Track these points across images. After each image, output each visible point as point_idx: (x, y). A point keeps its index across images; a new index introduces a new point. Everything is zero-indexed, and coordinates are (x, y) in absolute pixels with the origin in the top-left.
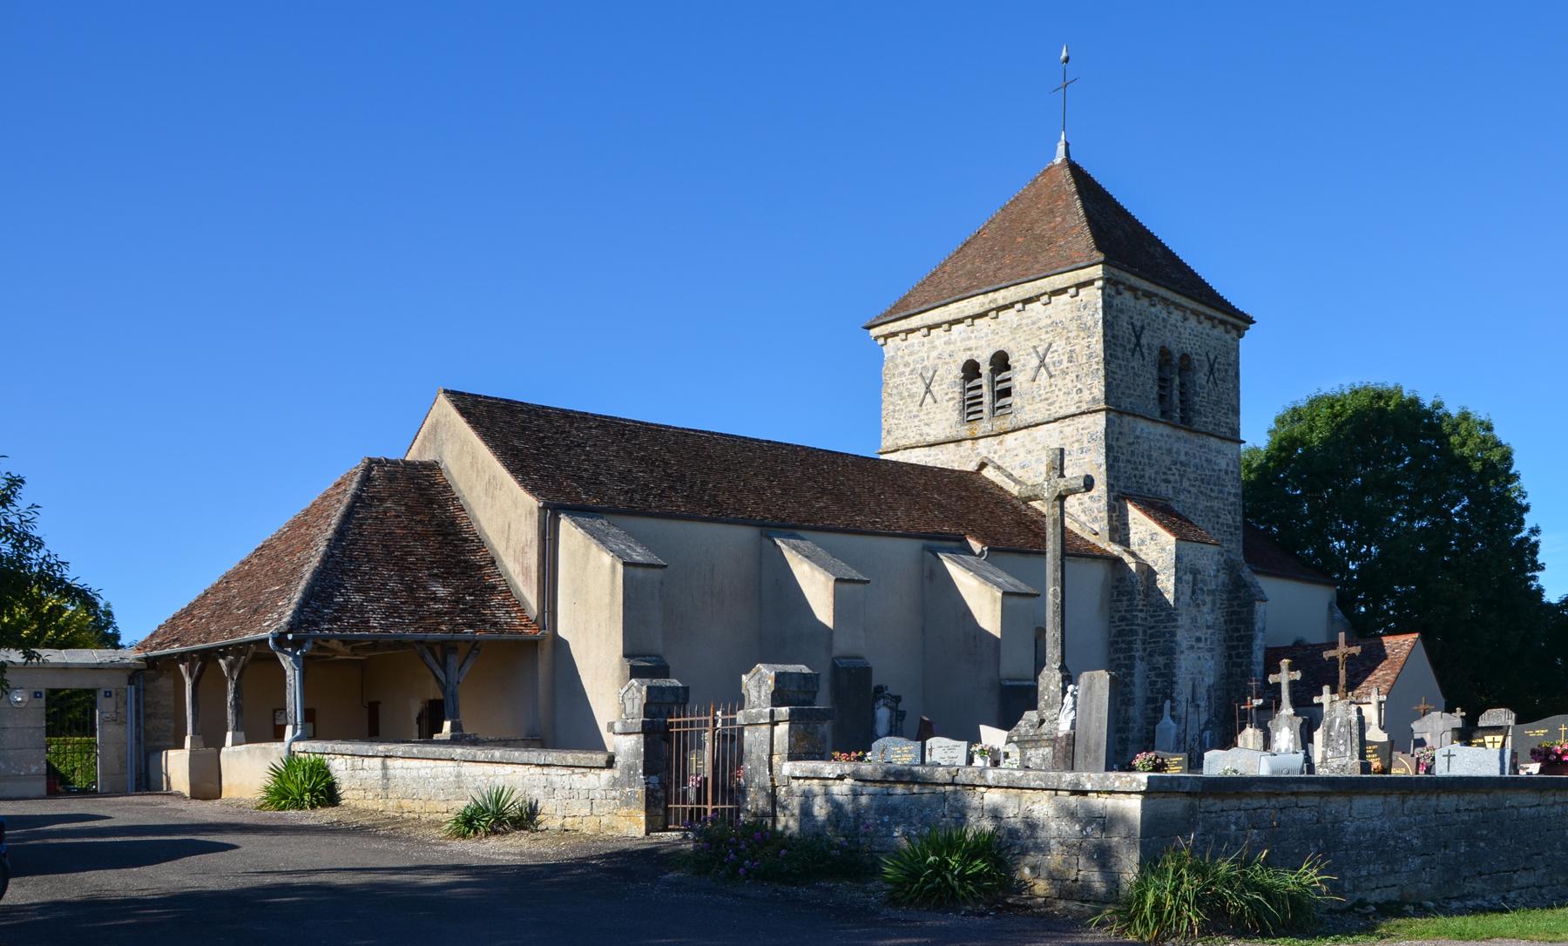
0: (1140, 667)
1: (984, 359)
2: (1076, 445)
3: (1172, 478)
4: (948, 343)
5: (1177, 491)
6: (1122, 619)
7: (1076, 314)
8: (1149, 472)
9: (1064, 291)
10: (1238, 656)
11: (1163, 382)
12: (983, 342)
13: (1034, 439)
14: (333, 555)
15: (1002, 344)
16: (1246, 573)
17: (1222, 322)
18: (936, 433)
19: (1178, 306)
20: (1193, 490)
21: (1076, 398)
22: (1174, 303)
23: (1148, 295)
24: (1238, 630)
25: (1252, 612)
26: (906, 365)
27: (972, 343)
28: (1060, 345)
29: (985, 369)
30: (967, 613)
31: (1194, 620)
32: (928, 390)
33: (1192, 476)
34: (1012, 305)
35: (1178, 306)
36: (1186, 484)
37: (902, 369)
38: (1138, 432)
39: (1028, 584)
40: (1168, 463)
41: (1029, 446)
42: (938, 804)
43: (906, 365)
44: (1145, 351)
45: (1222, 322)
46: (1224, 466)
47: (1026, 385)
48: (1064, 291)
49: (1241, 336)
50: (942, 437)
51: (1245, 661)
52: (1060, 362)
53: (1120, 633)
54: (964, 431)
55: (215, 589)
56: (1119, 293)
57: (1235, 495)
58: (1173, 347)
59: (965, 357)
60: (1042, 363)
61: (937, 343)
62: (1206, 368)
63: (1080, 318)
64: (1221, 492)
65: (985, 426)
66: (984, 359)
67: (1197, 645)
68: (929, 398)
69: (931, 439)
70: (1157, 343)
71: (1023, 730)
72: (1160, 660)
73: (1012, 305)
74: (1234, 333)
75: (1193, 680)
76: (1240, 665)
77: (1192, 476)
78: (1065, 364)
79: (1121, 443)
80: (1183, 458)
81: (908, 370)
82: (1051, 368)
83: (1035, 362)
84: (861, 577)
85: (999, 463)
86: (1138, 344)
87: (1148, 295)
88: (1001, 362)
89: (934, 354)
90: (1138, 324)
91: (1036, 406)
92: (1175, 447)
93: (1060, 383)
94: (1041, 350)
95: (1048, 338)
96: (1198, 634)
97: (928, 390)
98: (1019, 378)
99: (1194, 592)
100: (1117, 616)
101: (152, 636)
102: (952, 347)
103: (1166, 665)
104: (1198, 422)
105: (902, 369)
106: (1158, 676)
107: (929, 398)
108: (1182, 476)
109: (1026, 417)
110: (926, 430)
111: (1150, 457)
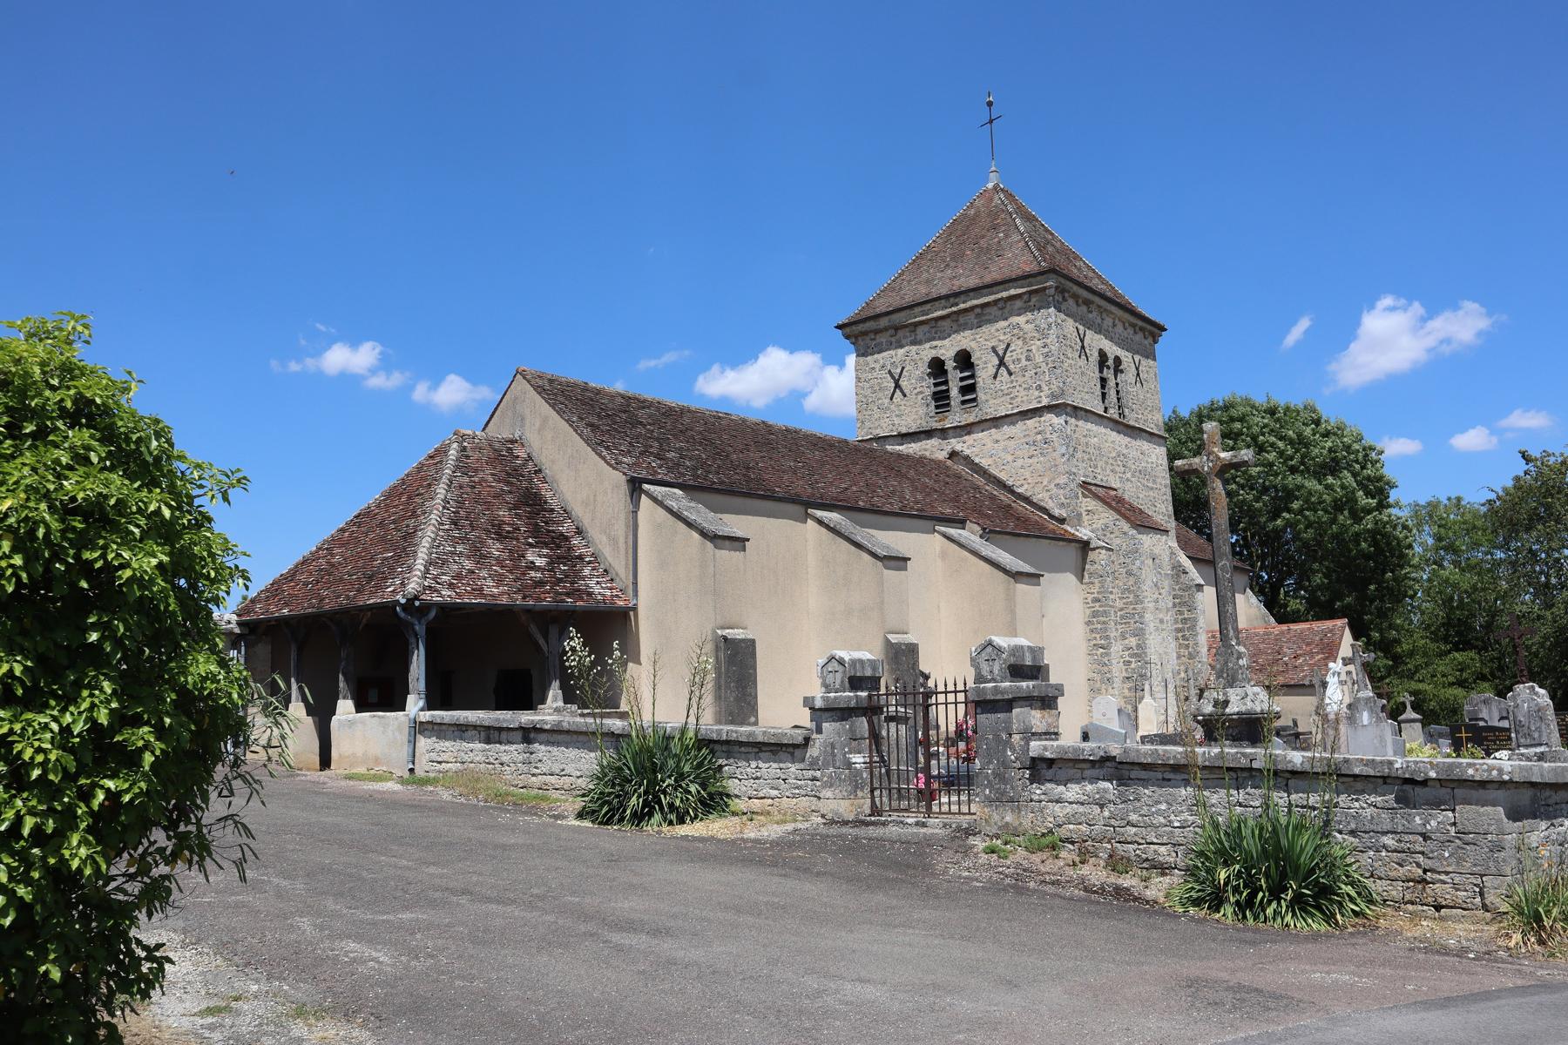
0: (1116, 648)
6: (1097, 600)
17: (1142, 329)
18: (909, 423)
28: (1017, 345)
29: (950, 365)
36: (1129, 475)
39: (1031, 565)
42: (413, 625)
45: (1142, 329)
49: (1155, 342)
52: (1019, 360)
53: (1095, 614)
55: (314, 557)
60: (1002, 363)
65: (957, 417)
71: (1534, 839)
72: (1133, 641)
74: (1150, 340)
82: (1012, 367)
84: (1028, 569)
93: (1021, 380)
97: (897, 386)
98: (984, 374)
100: (1090, 597)
101: (319, 549)
103: (1139, 646)
106: (1131, 656)
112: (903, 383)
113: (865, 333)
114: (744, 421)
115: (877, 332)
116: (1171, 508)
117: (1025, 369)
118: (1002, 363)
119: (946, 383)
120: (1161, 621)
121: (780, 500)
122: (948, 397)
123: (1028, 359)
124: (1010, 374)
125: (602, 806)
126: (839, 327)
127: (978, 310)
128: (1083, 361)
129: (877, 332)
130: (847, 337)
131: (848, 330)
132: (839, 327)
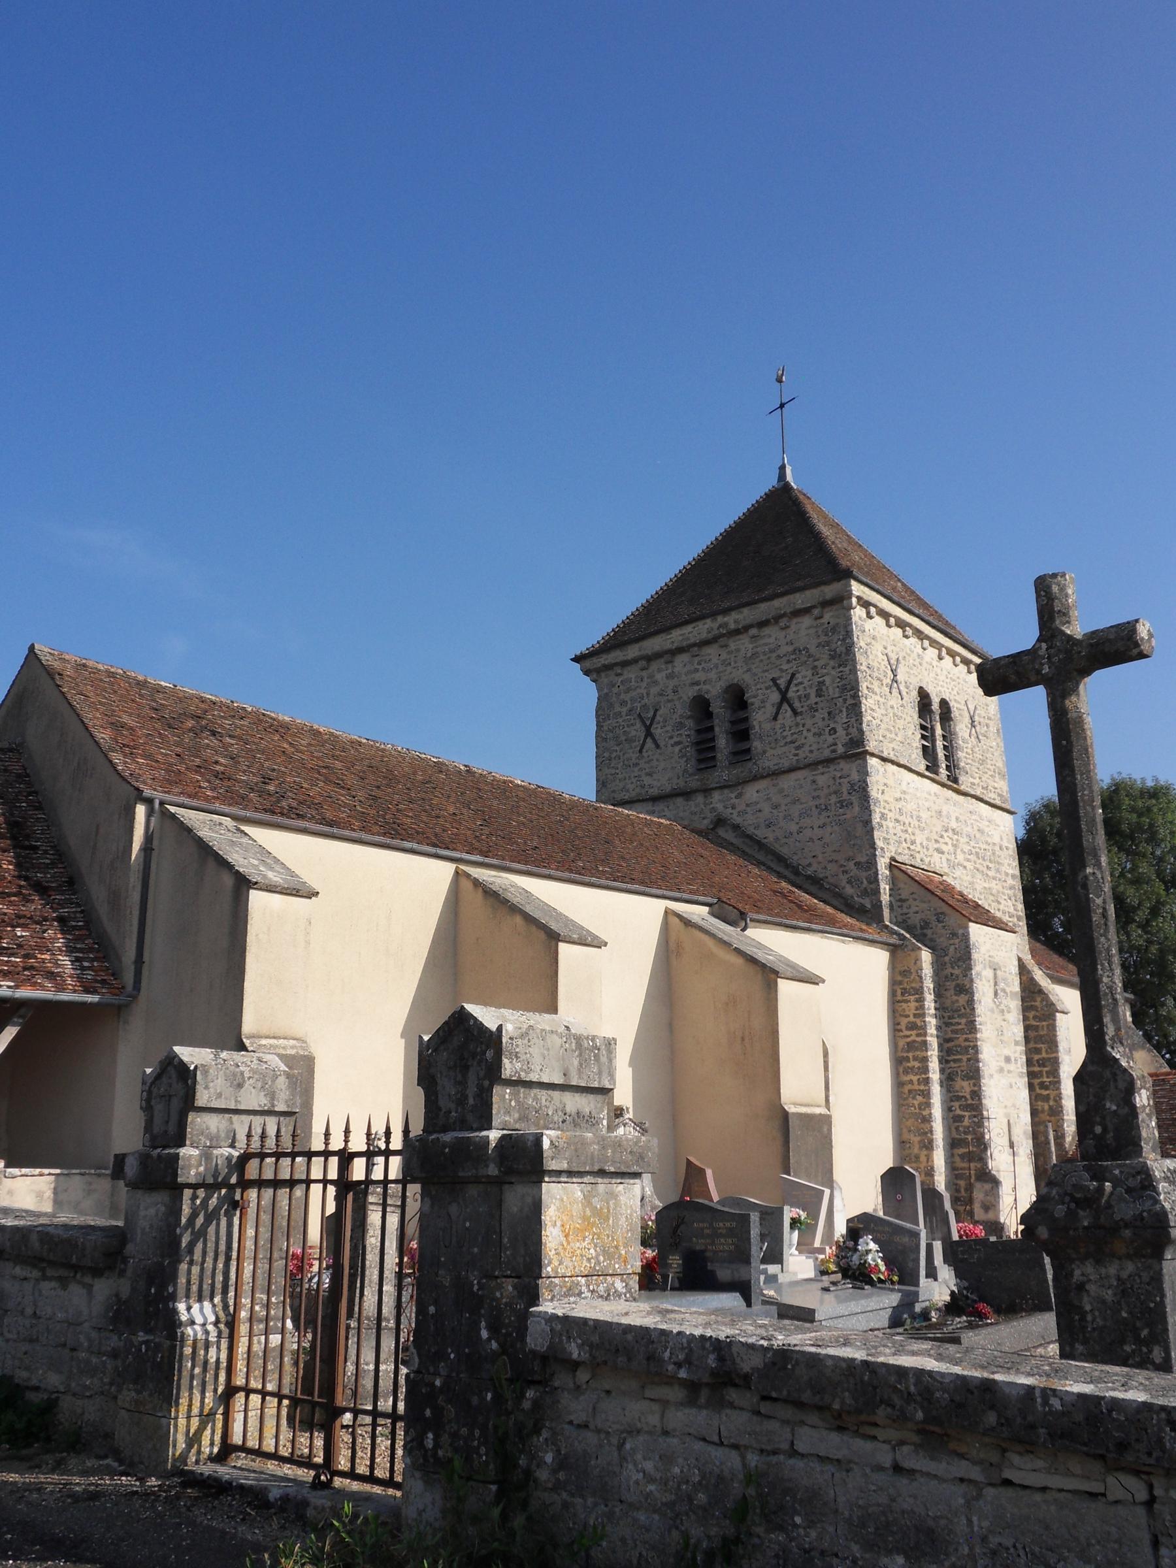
1: (714, 691)
2: (834, 799)
3: (945, 848)
4: (670, 676)
5: (953, 867)
7: (823, 638)
8: (920, 838)
9: (806, 611)
10: (1043, 1086)
11: (927, 733)
12: (713, 675)
13: (781, 791)
14: (967, 1077)
15: (738, 675)
16: (1039, 976)
19: (934, 643)
20: (969, 865)
21: (830, 739)
22: (928, 638)
23: (901, 624)
24: (1038, 1051)
25: (1052, 1028)
26: (623, 703)
27: (701, 676)
28: (805, 675)
29: (717, 707)
30: (182, 1045)
31: (1001, 1032)
32: (649, 734)
33: (966, 848)
34: (746, 628)
35: (934, 643)
36: (960, 857)
37: (618, 709)
38: (904, 787)
40: (939, 829)
41: (776, 799)
43: (623, 703)
44: (902, 688)
46: (996, 840)
47: (767, 726)
48: (806, 611)
50: (668, 789)
51: (1052, 1094)
52: (807, 696)
54: (694, 783)
56: (870, 617)
57: (1013, 876)
58: (931, 689)
59: (692, 692)
60: (784, 698)
61: (659, 677)
62: (967, 720)
63: (828, 643)
64: (998, 871)
65: (722, 774)
66: (714, 691)
67: (1007, 1067)
68: (649, 743)
69: (654, 792)
70: (915, 683)
73: (746, 628)
75: (1007, 1115)
76: (1046, 1098)
77: (966, 848)
78: (813, 699)
79: (886, 797)
80: (954, 824)
81: (624, 710)
82: (797, 704)
83: (775, 697)
85: (738, 820)
86: (894, 680)
87: (901, 624)
88: (738, 699)
89: (654, 690)
90: (893, 657)
91: (779, 751)
92: (945, 809)
93: (809, 722)
94: (782, 682)
95: (790, 668)
96: (1007, 1052)
98: (759, 719)
99: (996, 994)
102: (675, 682)
104: (965, 783)
105: (618, 709)
106: (963, 1108)
107: (649, 743)
108: (955, 846)
109: (769, 762)
110: (647, 780)
111: (919, 819)
112: (657, 731)
113: (608, 667)
114: (440, 767)
115: (625, 664)
116: (1021, 907)
117: (813, 709)
118: (784, 698)
119: (711, 729)
120: (1008, 1060)
121: (574, 943)
122: (713, 748)
123: (819, 694)
124: (795, 713)
125: (1116, 1542)
126: (577, 659)
127: (753, 631)
128: (894, 701)
129: (625, 664)
130: (587, 673)
131: (588, 664)
132: (577, 659)
